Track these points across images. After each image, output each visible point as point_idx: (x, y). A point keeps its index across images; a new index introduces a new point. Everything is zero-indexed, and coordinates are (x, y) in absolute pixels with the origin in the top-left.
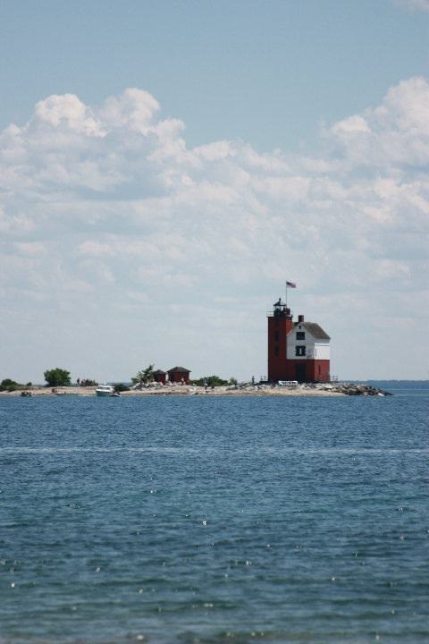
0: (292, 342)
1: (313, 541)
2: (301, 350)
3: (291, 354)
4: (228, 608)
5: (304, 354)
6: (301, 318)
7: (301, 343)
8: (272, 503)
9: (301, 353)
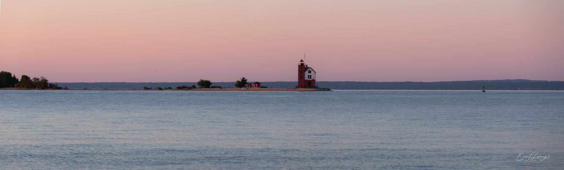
0: (307, 74)
1: (152, 149)
2: (310, 77)
3: (306, 78)
4: (509, 154)
5: (311, 78)
6: (307, 65)
7: (310, 74)
8: (74, 119)
9: (310, 77)
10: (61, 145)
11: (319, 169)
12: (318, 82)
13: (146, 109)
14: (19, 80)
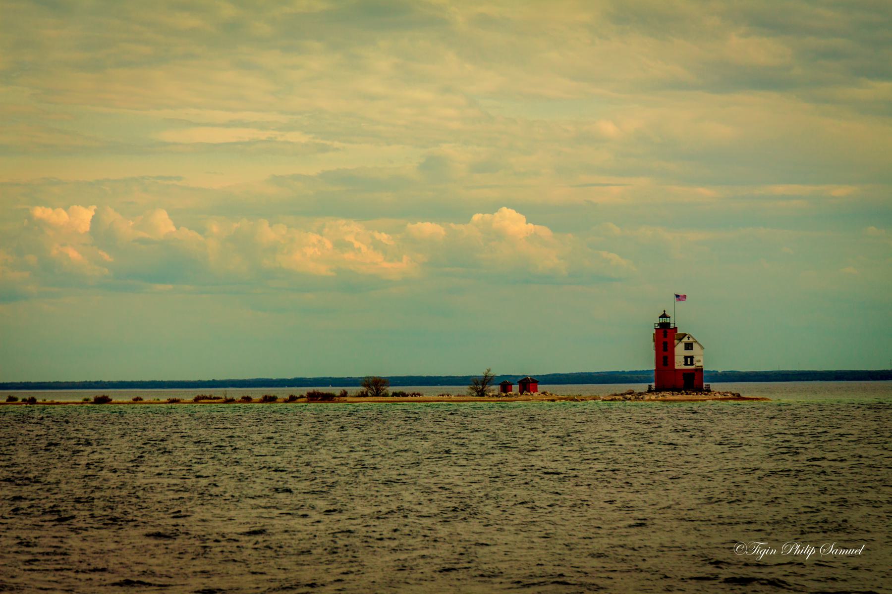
0: (680, 351)
2: (689, 360)
5: (692, 364)
7: (689, 353)
10: (139, 528)
11: (573, 589)
12: (707, 371)
13: (447, 487)
14: (95, 207)
